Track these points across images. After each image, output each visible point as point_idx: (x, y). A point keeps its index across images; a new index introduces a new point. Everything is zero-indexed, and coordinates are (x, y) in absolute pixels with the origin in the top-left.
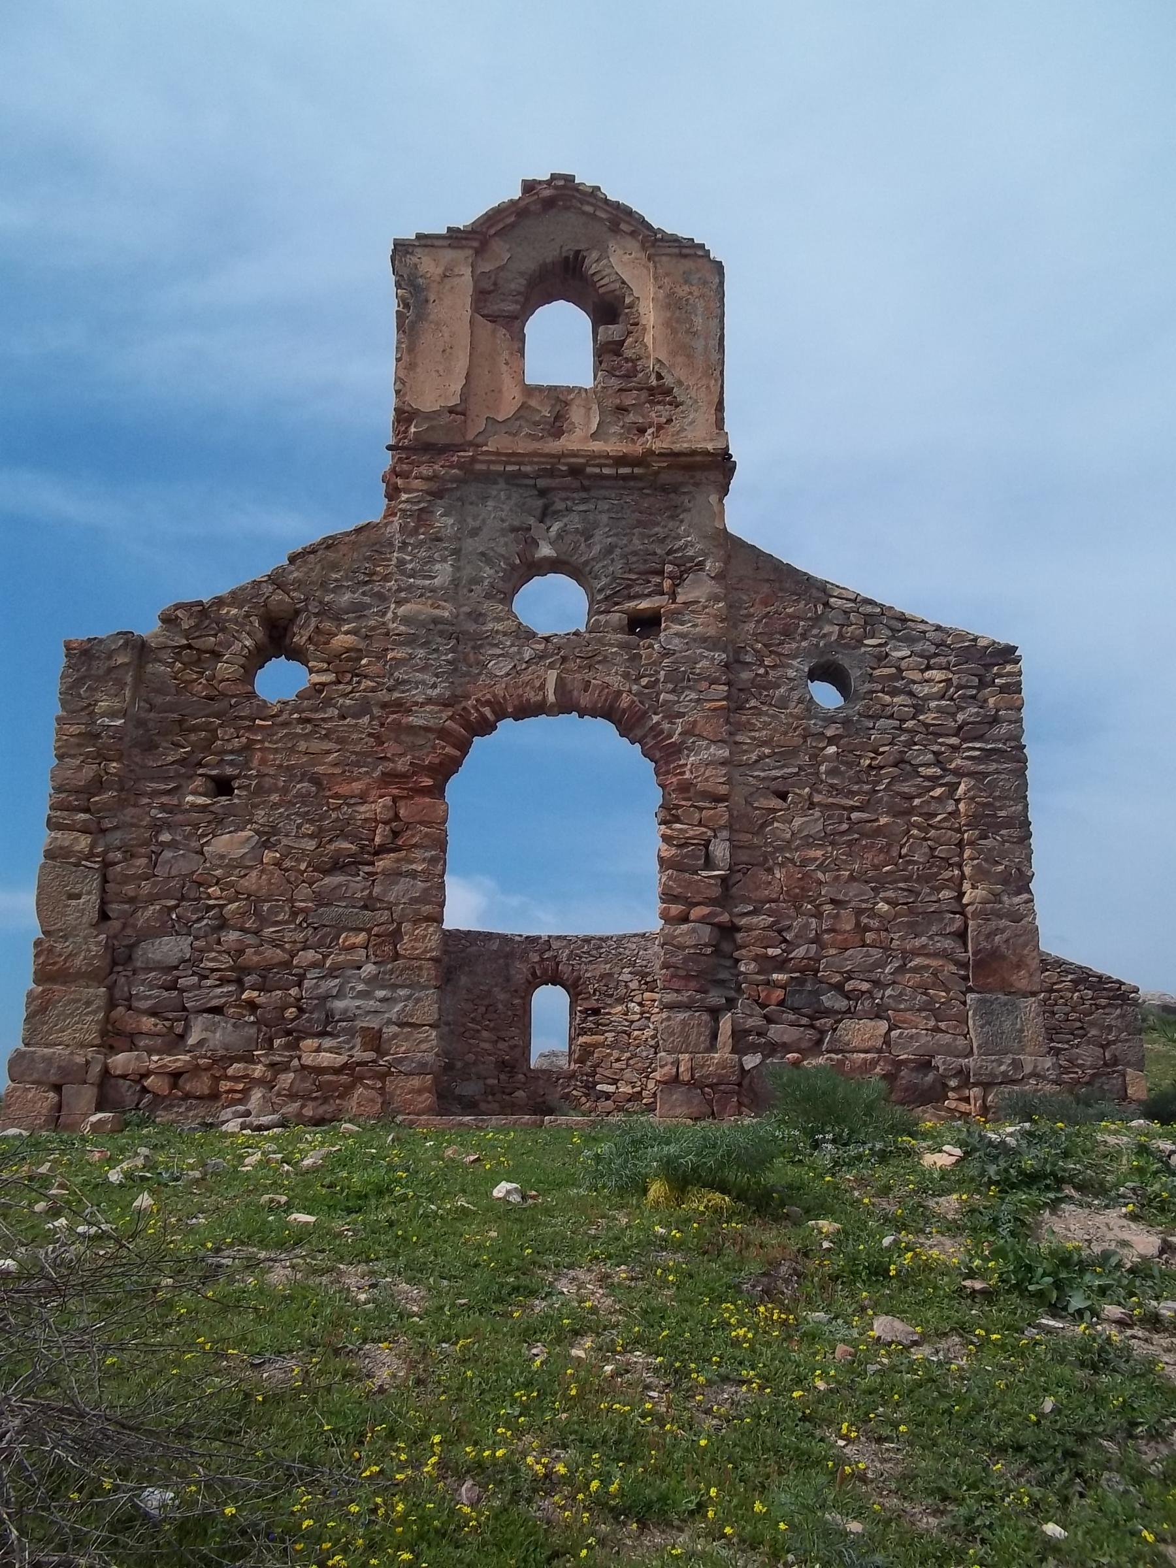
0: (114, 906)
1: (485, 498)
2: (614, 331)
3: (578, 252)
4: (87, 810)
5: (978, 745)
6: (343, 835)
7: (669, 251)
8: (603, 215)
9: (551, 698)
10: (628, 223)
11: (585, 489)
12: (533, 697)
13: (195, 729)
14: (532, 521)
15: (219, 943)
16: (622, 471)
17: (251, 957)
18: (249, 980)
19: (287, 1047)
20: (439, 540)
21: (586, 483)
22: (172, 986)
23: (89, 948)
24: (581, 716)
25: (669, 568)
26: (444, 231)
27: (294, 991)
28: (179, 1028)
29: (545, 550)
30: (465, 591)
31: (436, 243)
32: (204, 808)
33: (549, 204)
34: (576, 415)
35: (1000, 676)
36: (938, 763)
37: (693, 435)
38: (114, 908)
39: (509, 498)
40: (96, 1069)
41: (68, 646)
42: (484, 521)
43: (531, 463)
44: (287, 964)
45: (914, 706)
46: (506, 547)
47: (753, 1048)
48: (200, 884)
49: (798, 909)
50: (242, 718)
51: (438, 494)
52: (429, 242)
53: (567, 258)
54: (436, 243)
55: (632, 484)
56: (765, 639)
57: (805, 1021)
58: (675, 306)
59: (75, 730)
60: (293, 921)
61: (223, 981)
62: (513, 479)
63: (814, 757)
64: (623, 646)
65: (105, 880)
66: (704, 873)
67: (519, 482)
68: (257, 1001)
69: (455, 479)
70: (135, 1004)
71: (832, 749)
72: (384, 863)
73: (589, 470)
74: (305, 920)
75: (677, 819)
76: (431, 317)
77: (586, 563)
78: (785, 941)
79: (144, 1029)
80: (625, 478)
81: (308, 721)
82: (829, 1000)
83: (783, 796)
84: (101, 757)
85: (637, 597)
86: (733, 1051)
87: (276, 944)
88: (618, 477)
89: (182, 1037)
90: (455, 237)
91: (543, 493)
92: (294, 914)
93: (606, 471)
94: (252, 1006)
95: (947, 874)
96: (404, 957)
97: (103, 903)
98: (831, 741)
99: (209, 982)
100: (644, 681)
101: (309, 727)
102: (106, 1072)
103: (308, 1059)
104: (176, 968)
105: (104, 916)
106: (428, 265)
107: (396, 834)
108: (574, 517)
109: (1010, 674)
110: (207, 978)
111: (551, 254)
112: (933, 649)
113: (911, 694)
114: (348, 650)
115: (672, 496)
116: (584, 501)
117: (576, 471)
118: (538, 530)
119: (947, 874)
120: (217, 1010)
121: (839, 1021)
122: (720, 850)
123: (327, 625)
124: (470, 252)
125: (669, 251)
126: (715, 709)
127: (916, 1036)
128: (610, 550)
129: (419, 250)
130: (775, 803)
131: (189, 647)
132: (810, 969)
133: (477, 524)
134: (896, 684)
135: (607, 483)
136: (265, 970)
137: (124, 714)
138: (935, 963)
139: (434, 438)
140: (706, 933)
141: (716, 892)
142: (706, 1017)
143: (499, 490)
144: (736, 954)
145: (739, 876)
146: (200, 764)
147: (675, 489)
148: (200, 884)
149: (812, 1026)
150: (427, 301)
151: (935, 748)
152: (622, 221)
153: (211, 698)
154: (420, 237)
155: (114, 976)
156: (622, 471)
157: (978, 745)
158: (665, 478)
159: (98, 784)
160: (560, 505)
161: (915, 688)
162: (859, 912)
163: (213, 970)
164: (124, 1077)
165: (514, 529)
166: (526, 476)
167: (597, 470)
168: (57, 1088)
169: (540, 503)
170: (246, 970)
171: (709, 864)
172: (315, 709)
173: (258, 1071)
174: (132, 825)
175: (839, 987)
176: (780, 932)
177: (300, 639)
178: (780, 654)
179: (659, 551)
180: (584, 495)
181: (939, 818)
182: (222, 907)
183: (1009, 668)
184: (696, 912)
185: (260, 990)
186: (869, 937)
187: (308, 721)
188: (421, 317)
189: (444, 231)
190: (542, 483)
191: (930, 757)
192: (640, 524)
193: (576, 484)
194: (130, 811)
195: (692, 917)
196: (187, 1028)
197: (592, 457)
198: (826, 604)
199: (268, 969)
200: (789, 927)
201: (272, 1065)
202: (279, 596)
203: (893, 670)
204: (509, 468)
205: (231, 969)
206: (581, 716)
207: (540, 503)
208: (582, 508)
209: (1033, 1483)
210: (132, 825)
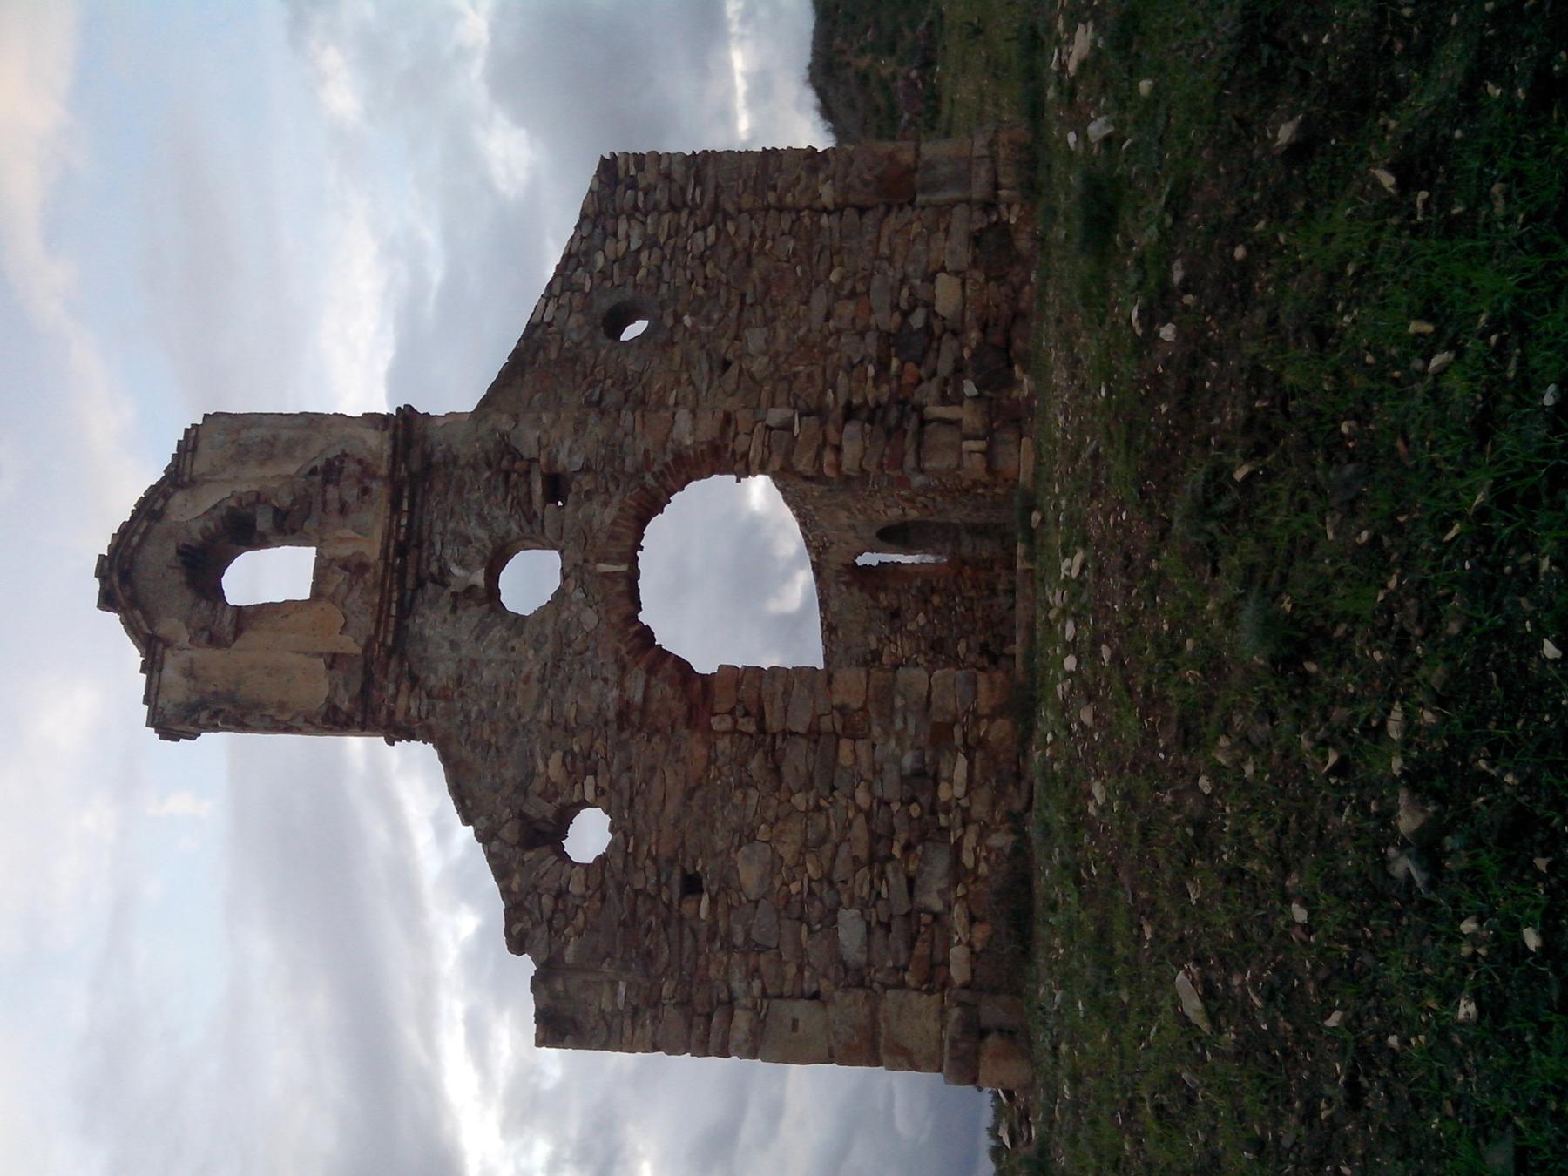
0: (806, 986)
1: (422, 638)
2: (264, 522)
3: (179, 552)
4: (709, 1017)
5: (690, 191)
6: (743, 765)
7: (188, 462)
8: (145, 524)
9: (624, 568)
10: (155, 501)
11: (419, 546)
12: (622, 586)
13: (633, 911)
14: (447, 593)
15: (844, 882)
16: (405, 506)
17: (862, 852)
18: (882, 852)
19: (947, 812)
20: (460, 678)
21: (414, 542)
22: (887, 927)
23: (848, 1008)
24: (641, 548)
25: (505, 464)
26: (144, 676)
27: (895, 807)
28: (926, 918)
29: (479, 578)
30: (514, 654)
31: (155, 685)
32: (713, 902)
33: (126, 577)
34: (345, 551)
35: (627, 170)
36: (704, 228)
37: (377, 443)
38: (809, 987)
39: (423, 616)
40: (965, 995)
41: (541, 1042)
42: (445, 638)
43: (391, 591)
44: (869, 816)
45: (651, 248)
46: (472, 616)
47: (958, 388)
48: (788, 902)
49: (831, 351)
50: (625, 866)
51: (415, 680)
52: (153, 692)
53: (184, 563)
54: (155, 685)
55: (418, 499)
56: (579, 378)
57: (935, 345)
58: (242, 454)
59: (628, 1032)
60: (827, 809)
61: (882, 875)
62: (406, 611)
63: (692, 336)
64: (578, 506)
65: (780, 996)
66: (797, 430)
67: (408, 597)
68: (903, 842)
69: (401, 664)
70: (902, 962)
71: (687, 320)
72: (773, 722)
73: (402, 538)
74: (826, 799)
75: (745, 455)
76: (233, 688)
77: (493, 543)
78: (861, 362)
79: (928, 951)
80: (412, 505)
81: (632, 801)
82: (917, 319)
83: (726, 365)
84: (655, 1003)
85: (529, 494)
86: (961, 404)
87: (849, 825)
88: (411, 512)
89: (936, 917)
90: (151, 666)
91: (420, 584)
92: (818, 808)
93: (404, 522)
94: (908, 848)
95: (807, 221)
96: (865, 702)
97: (802, 996)
98: (678, 319)
99: (884, 891)
100: (612, 488)
101: (637, 799)
102: (966, 986)
103: (959, 791)
104: (868, 923)
105: (815, 996)
106: (177, 688)
107: (747, 714)
108: (448, 552)
109: (627, 161)
110: (879, 893)
111: (178, 577)
112: (599, 231)
113: (639, 251)
114: (564, 763)
115: (435, 459)
116: (432, 545)
117: (402, 550)
118: (456, 586)
119: (807, 221)
120: (911, 882)
121: (936, 314)
122: (775, 416)
123: (538, 785)
124: (168, 652)
125: (188, 462)
126: (644, 423)
127: (954, 249)
128: (481, 518)
129: (160, 703)
130: (733, 371)
131: (550, 921)
132: (886, 338)
133: (447, 644)
134: (629, 261)
135: (416, 523)
136: (875, 838)
137: (614, 984)
138: (886, 232)
139: (356, 688)
140: (852, 428)
141: (813, 421)
142: (929, 428)
143: (414, 624)
144: (872, 404)
145: (800, 403)
146: (668, 906)
147: (427, 457)
148: (788, 902)
149: (940, 338)
150: (215, 693)
151: (690, 230)
152: (150, 508)
153: (603, 898)
154: (146, 700)
155: (875, 985)
156: (405, 506)
157: (690, 191)
158: (416, 465)
159: (685, 1003)
160: (434, 568)
161: (634, 247)
162: (838, 298)
163: (872, 887)
164: (973, 971)
165: (454, 609)
166: (402, 597)
167: (403, 530)
168: (983, 1033)
169: (429, 585)
170: (872, 859)
171: (787, 427)
172: (620, 793)
173: (970, 840)
174: (726, 972)
175: (906, 315)
176: (853, 366)
177: (549, 810)
178: (594, 367)
179: (487, 474)
180: (426, 545)
181: (754, 226)
182: (810, 880)
183: (621, 162)
184: (833, 437)
185: (892, 841)
186: (860, 288)
187: (632, 801)
188: (231, 697)
189: (144, 676)
190: (410, 582)
191: (699, 234)
192: (459, 492)
193: (415, 553)
194: (712, 972)
195: (836, 442)
196: (927, 911)
197: (388, 536)
198: (550, 324)
199: (871, 832)
200: (849, 358)
201: (964, 825)
202: (505, 833)
203: (616, 267)
204: (394, 611)
205: (871, 869)
206: (641, 548)
207: (429, 585)
208: (438, 547)
209: (1363, 1114)
210: (726, 972)
